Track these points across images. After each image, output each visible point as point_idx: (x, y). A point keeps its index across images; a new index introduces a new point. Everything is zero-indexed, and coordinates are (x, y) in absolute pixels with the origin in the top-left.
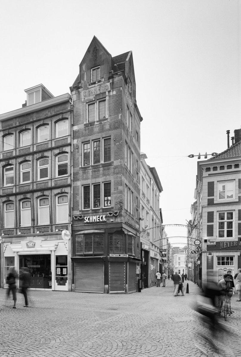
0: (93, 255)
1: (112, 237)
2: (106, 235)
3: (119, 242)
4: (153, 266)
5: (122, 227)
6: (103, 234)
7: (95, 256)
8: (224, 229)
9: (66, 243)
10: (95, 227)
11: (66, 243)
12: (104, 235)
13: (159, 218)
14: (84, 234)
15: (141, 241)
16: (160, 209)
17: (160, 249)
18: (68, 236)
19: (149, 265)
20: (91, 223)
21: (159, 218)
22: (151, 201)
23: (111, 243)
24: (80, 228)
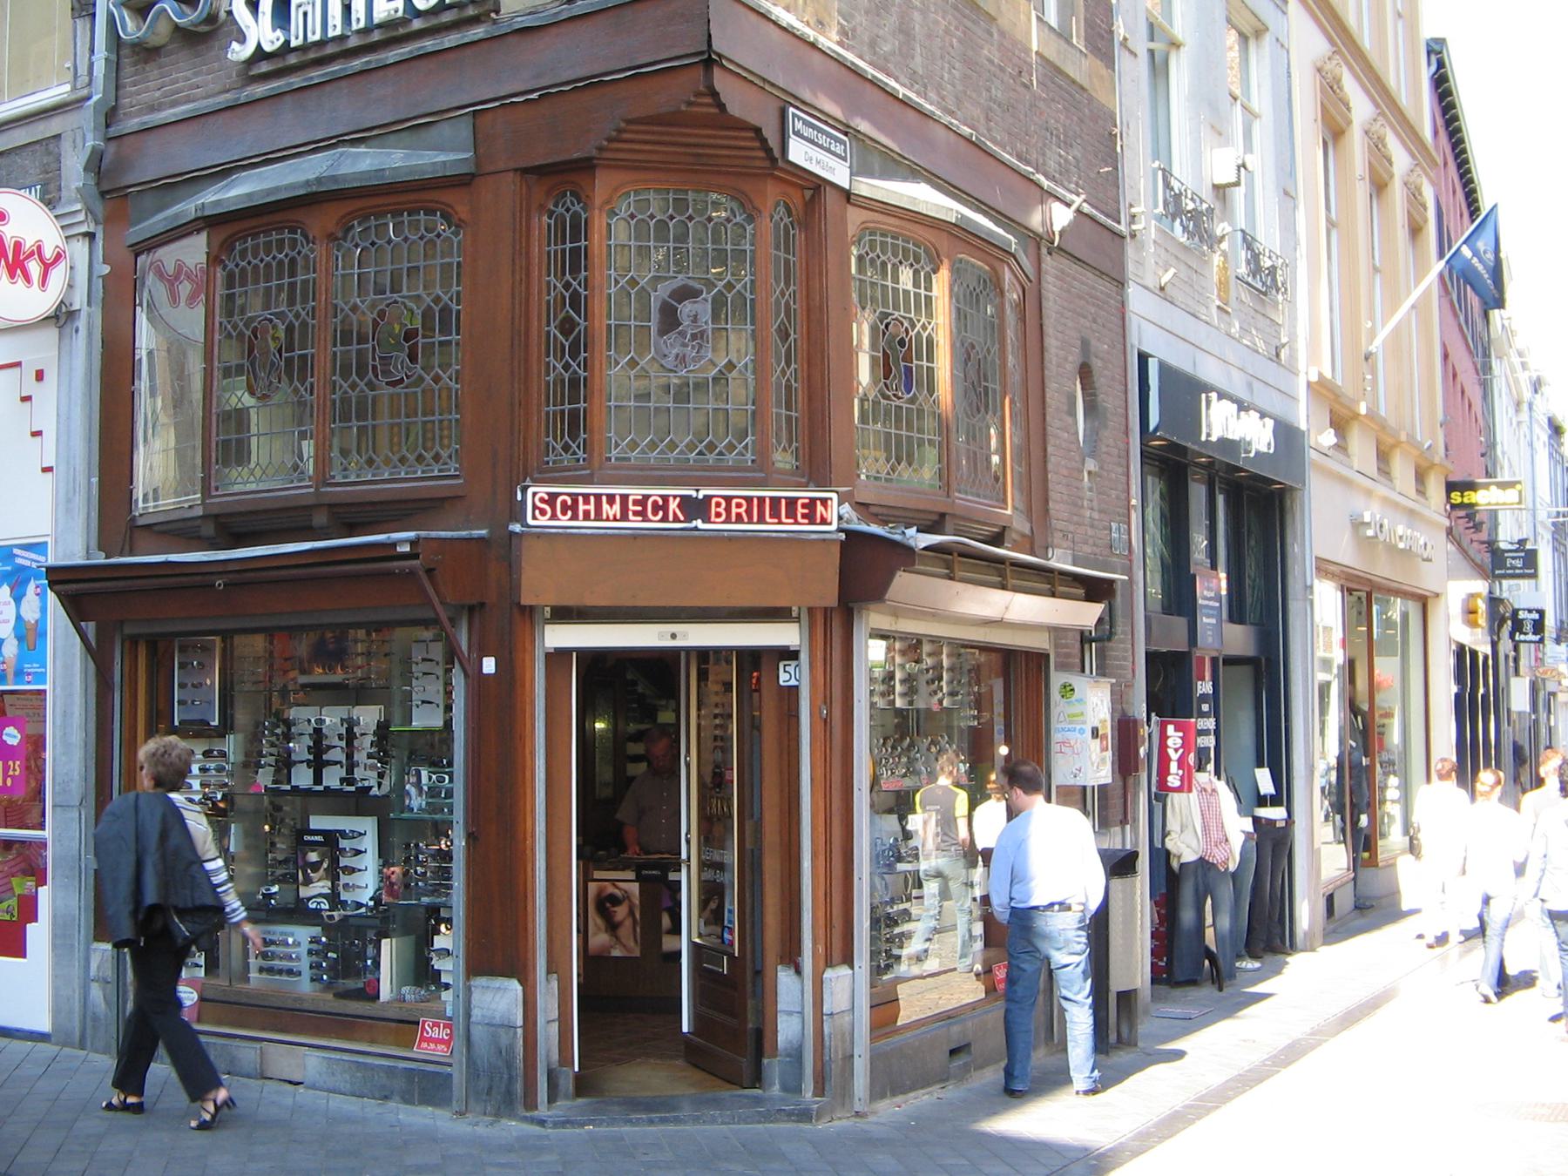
0: (320, 519)
1: (578, 229)
2: (504, 193)
3: (686, 309)
4: (952, 694)
5: (710, 61)
6: (448, 197)
7: (352, 530)
8: (1058, 803)
9: (40, 376)
10: (343, 111)
11: (40, 376)
12: (462, 211)
13: (1427, 134)
14: (209, 222)
15: (1162, 349)
16: (1436, 50)
17: (1451, 487)
18: (34, 268)
19: (1294, 587)
20: (319, 54)
21: (1427, 134)
22: (1366, 32)
23: (567, 327)
24: (187, 154)
